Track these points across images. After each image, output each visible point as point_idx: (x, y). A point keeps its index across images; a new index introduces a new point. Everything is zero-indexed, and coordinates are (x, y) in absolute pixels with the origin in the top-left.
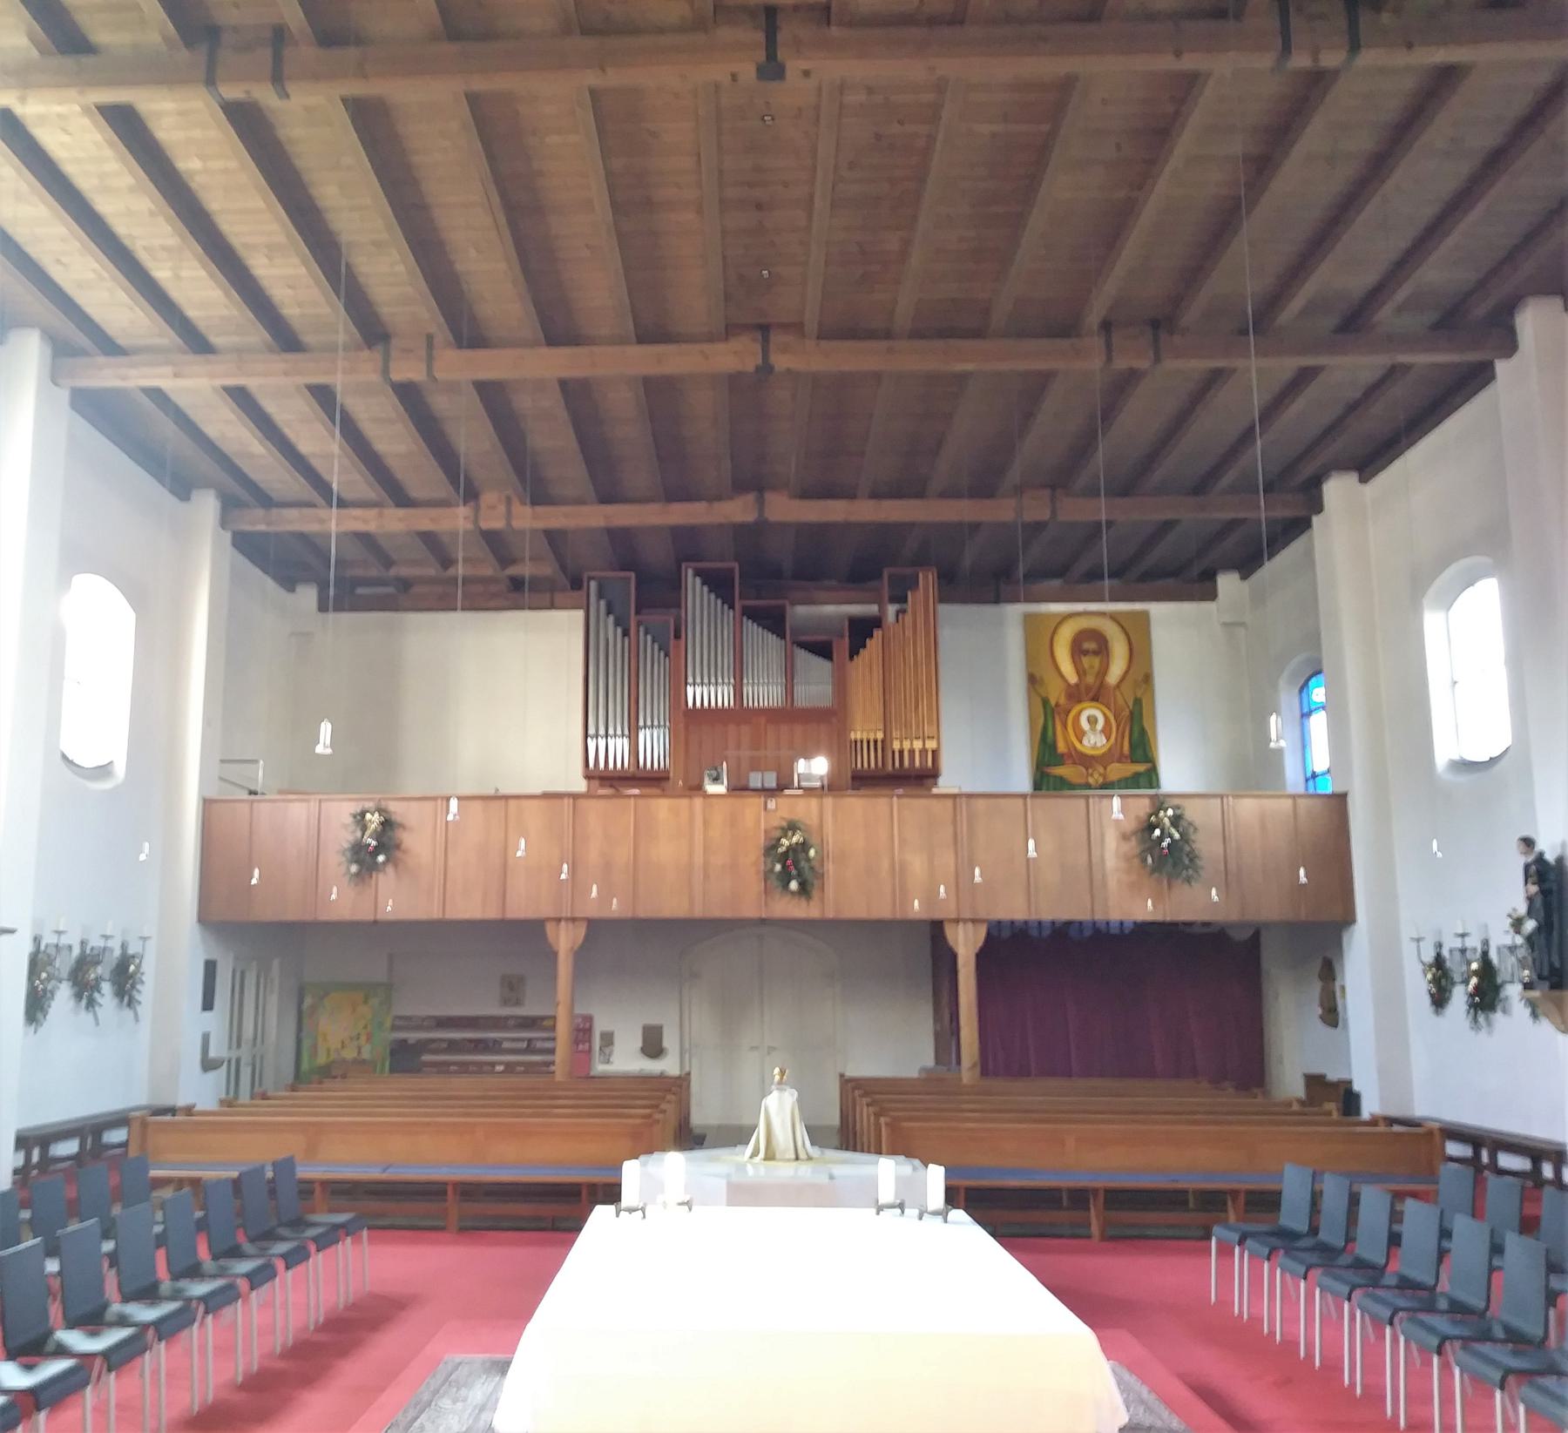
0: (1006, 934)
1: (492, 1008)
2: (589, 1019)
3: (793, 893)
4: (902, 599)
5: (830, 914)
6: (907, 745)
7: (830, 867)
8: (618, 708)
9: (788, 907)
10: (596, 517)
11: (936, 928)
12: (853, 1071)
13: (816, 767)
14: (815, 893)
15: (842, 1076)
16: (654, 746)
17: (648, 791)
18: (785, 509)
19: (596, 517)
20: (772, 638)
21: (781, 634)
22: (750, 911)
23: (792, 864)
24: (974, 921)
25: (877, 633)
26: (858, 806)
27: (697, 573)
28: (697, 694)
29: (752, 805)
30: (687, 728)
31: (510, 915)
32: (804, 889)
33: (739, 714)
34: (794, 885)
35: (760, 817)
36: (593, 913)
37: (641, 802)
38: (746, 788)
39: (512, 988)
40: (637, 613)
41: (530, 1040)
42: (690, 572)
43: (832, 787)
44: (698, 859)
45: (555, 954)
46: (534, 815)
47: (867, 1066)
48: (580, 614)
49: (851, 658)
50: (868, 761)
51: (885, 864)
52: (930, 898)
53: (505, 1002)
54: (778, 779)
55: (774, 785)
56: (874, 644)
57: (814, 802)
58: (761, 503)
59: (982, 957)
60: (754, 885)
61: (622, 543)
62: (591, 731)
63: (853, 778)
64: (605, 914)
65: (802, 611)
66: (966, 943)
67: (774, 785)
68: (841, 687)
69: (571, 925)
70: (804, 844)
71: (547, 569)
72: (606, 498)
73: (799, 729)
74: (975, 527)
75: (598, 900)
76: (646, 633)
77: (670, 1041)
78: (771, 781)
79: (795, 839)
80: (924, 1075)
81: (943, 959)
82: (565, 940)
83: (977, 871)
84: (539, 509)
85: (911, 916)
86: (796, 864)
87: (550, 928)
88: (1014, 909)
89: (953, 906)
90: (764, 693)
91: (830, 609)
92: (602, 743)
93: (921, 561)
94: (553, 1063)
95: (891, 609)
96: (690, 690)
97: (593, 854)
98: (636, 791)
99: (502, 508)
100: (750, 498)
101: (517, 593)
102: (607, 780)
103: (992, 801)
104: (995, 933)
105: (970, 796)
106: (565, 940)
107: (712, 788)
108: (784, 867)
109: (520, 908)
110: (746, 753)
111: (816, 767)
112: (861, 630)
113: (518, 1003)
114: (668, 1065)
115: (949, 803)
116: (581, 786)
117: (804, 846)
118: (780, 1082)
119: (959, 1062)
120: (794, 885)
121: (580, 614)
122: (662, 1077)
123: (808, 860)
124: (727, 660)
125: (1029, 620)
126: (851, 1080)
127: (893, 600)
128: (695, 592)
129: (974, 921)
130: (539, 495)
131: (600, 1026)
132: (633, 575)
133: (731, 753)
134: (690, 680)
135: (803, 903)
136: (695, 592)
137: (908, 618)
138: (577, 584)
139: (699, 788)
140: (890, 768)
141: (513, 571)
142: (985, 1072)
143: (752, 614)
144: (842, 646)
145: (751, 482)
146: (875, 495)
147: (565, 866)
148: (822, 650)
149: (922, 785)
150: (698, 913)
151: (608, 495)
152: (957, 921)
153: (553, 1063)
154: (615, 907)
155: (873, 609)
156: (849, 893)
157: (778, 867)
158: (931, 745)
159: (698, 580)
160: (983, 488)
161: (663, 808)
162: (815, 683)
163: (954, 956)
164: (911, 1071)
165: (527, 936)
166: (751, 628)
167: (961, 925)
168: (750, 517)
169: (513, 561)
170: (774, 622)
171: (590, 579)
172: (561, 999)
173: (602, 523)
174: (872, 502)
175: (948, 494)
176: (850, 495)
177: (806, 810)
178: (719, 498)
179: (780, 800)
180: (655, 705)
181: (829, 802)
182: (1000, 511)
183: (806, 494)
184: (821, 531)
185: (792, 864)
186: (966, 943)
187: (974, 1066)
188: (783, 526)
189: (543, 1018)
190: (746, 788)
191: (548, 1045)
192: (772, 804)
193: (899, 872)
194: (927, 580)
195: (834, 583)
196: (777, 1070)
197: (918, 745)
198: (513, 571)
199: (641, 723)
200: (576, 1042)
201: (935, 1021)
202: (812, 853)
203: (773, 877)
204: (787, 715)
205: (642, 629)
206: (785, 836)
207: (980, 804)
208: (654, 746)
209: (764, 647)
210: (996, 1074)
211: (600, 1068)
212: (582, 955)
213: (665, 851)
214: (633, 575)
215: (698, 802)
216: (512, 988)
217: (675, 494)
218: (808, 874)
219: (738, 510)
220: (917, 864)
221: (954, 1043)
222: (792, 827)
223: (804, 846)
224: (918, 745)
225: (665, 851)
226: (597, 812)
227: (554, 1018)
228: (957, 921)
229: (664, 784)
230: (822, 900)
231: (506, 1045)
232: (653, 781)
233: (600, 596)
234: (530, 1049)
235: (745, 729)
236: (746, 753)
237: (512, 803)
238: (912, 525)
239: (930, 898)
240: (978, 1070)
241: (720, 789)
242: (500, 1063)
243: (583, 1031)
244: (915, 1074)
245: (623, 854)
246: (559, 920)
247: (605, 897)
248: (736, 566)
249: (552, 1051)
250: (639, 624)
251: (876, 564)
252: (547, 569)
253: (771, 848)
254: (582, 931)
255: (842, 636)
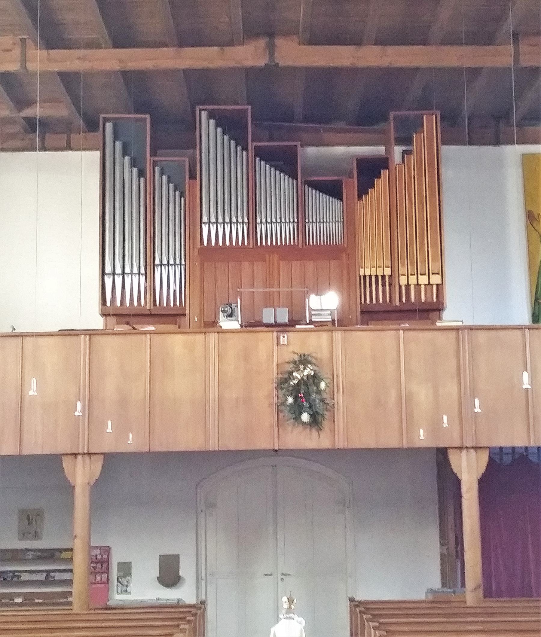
0: (508, 459)
1: (16, 544)
2: (107, 550)
3: (303, 423)
4: (406, 140)
5: (340, 444)
6: (413, 280)
7: (340, 399)
8: (134, 248)
9: (310, 440)
10: (111, 60)
11: (442, 453)
12: (361, 596)
13: (326, 302)
14: (326, 424)
15: (351, 600)
16: (170, 281)
17: (162, 327)
18: (294, 54)
19: (111, 60)
20: (285, 181)
21: (293, 175)
22: (263, 443)
23: (303, 397)
24: (476, 448)
25: (384, 173)
26: (367, 340)
27: (211, 115)
28: (210, 232)
29: (265, 340)
30: (202, 266)
31: (25, 452)
32: (316, 421)
33: (254, 251)
34: (305, 417)
35: (271, 352)
36: (107, 448)
37: (157, 338)
38: (259, 324)
39: (30, 522)
40: (154, 154)
41: (48, 572)
42: (204, 114)
43: (341, 322)
44: (213, 394)
45: (72, 488)
46: (51, 354)
47: (381, 586)
48: (96, 155)
49: (360, 197)
50: (377, 296)
51: (393, 393)
52: (435, 427)
53: (23, 536)
54: (291, 313)
55: (286, 321)
56: (381, 183)
57: (324, 336)
58: (271, 48)
59: (484, 483)
60: (269, 417)
61: (136, 84)
62: (108, 269)
63: (362, 312)
64: (122, 448)
65: (311, 151)
66: (469, 469)
67: (286, 321)
68: (350, 223)
69: (87, 458)
70: (315, 376)
71: (62, 111)
72: (119, 42)
73: (310, 266)
74: (475, 72)
75: (112, 436)
76: (162, 174)
77: (186, 570)
78: (283, 317)
79: (306, 373)
80: (431, 598)
81: (448, 484)
82: (82, 475)
83: (477, 401)
84: (51, 51)
85: (417, 445)
86: (307, 395)
87: (67, 463)
88: (514, 436)
89: (456, 434)
90: (277, 228)
91: (340, 150)
92: (119, 280)
93: (425, 105)
94: (70, 594)
95: (398, 150)
96: (205, 229)
97: (109, 388)
98: (151, 328)
99: (17, 52)
100: (262, 42)
101: (40, 134)
102: (123, 317)
103: (493, 333)
104: (497, 459)
105: (471, 329)
106: (82, 475)
107: (226, 324)
108: (296, 399)
109: (36, 445)
110: (259, 289)
111: (326, 302)
112: (370, 170)
113: (36, 536)
114: (185, 594)
115: (452, 335)
116: (97, 322)
117: (315, 378)
118: (289, 610)
119: (463, 585)
120: (305, 417)
121: (96, 155)
122: (178, 605)
123: (319, 392)
124: (241, 200)
125: (527, 161)
126: (361, 603)
127: (399, 141)
128: (209, 132)
129: (476, 448)
130: (53, 37)
131: (116, 558)
132: (148, 116)
133: (245, 290)
134: (205, 219)
135: (315, 433)
136: (209, 132)
137: (413, 159)
138: (92, 124)
139: (214, 323)
140: (398, 303)
141: (27, 112)
142: (488, 593)
143: (263, 154)
144: (351, 186)
145: (264, 29)
146: (382, 41)
147: (79, 404)
148: (333, 190)
149: (428, 318)
150: (213, 446)
151: (122, 39)
152: (461, 448)
153: (70, 594)
154: (132, 443)
155: (381, 150)
156: (354, 426)
157: (290, 400)
158: (436, 279)
159: (212, 122)
160: (482, 34)
161: (178, 344)
162: (326, 217)
163: (458, 482)
164: (419, 594)
165: (48, 468)
166: (263, 166)
167: (464, 452)
168: (262, 62)
169: (30, 103)
170: (286, 162)
171: (106, 120)
172: (78, 534)
173: (117, 66)
174: (378, 48)
175: (449, 40)
176: (356, 41)
177: (316, 344)
178: (231, 43)
179: (291, 334)
180: (170, 246)
181: (338, 335)
182: (499, 57)
183: (314, 40)
184: (329, 75)
185: (303, 397)
186: (469, 469)
187: (476, 588)
188: (293, 70)
189: (61, 551)
190: (259, 324)
191: (66, 576)
192: (283, 340)
193: (405, 402)
194: (431, 122)
195: (342, 125)
196: (285, 599)
197: (423, 280)
198: (27, 112)
199: (157, 262)
200: (94, 573)
201: (441, 544)
202: (323, 385)
203: (286, 410)
204: (300, 251)
205: (157, 169)
206: (298, 370)
207: (482, 336)
208: (170, 281)
209: (277, 187)
210: (500, 595)
211: (117, 598)
212: (97, 488)
213: (181, 386)
214: (148, 116)
215: (213, 338)
216: (30, 522)
217: (187, 39)
218: (319, 406)
219: (249, 55)
220: (422, 394)
221: (459, 564)
222: (304, 361)
223: (315, 378)
224: (423, 280)
225: (181, 386)
226: (112, 348)
227: (71, 550)
228: (461, 448)
229: (182, 320)
230: (333, 431)
231: (25, 577)
232: (169, 317)
233: (116, 138)
234: (48, 581)
235: (259, 267)
236: (259, 289)
237: (28, 340)
238: (416, 70)
239: (435, 427)
240: (481, 591)
241: (233, 324)
242: (18, 595)
243: (100, 562)
244: (422, 596)
245: (138, 390)
246: (75, 455)
247: (122, 429)
248: (249, 107)
249: (69, 582)
250: (155, 164)
251: (378, 106)
252: (62, 111)
253: (282, 383)
254: (98, 465)
255: (351, 176)
